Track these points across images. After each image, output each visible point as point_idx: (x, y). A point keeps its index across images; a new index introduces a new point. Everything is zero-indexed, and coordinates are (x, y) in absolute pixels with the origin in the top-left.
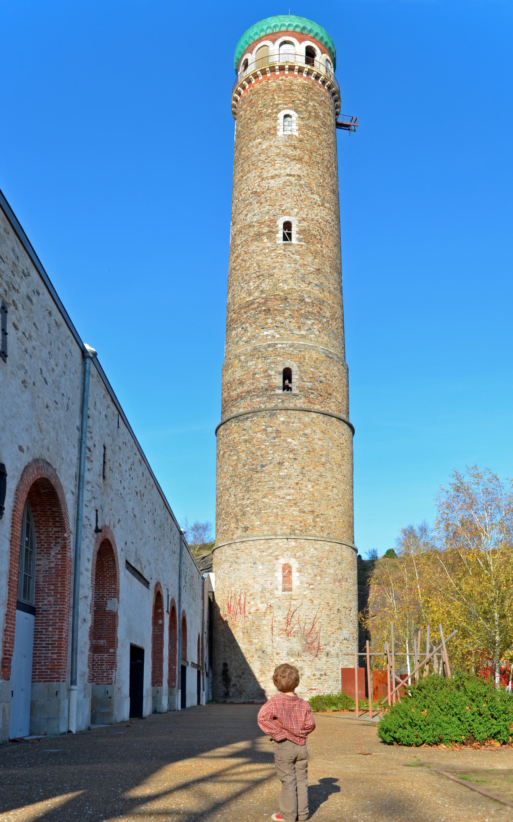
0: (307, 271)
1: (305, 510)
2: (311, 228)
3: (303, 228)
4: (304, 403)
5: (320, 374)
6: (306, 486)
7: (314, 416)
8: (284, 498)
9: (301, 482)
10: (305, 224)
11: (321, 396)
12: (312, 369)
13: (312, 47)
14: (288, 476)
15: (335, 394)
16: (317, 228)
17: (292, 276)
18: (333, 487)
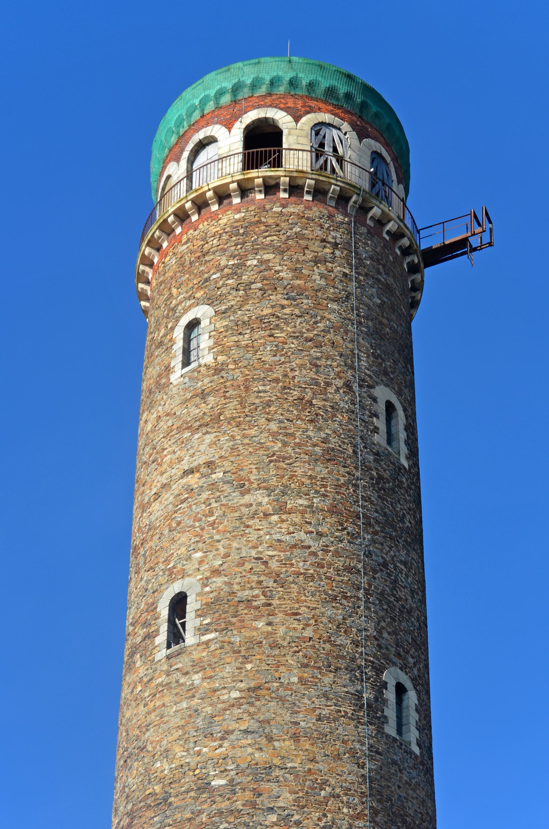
2: (236, 587)
3: (214, 594)
10: (219, 581)
13: (266, 119)
16: (255, 578)
17: (180, 732)
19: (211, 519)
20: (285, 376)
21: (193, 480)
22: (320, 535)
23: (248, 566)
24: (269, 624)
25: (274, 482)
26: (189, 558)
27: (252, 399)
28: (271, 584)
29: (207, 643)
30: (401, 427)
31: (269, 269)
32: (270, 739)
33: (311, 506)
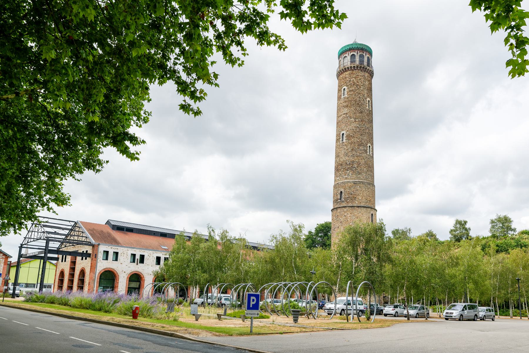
21: (345, 115)
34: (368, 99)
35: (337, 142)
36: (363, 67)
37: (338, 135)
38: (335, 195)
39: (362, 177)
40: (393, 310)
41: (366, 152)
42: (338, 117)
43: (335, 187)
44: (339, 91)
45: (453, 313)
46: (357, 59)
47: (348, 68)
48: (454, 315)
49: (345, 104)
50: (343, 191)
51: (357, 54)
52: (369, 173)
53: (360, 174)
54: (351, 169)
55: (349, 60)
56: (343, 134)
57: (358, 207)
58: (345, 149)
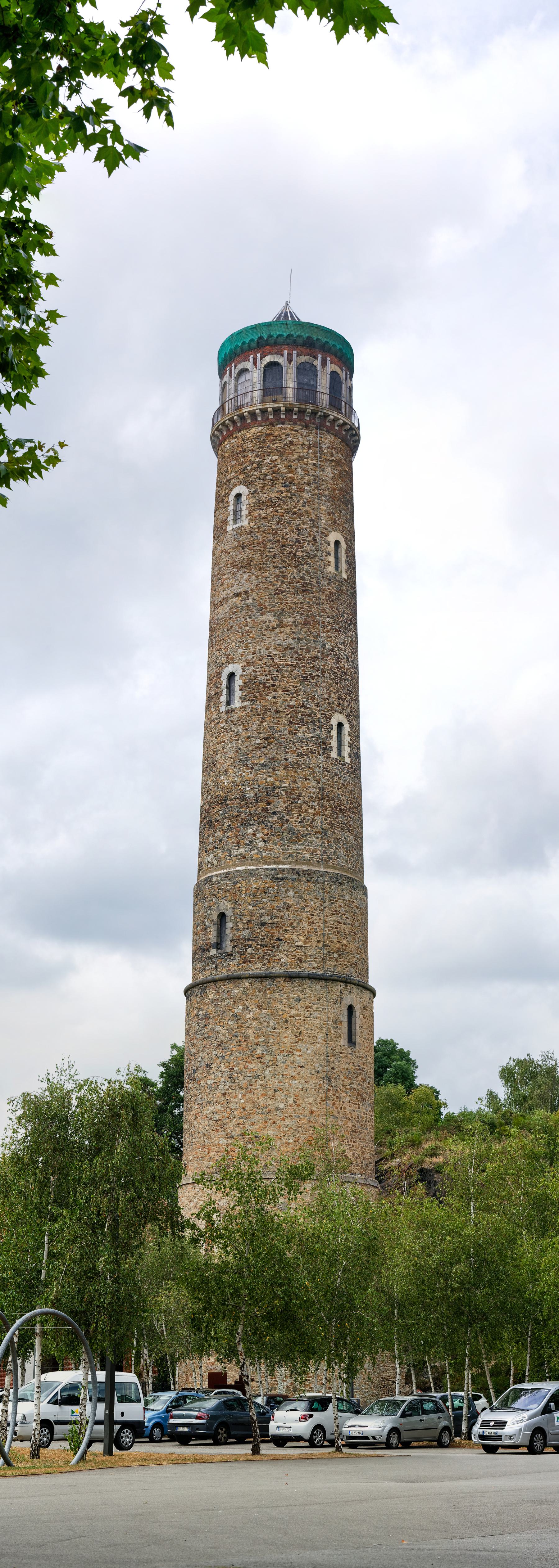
0: (251, 748)
1: (234, 1133)
4: (239, 965)
5: (262, 911)
6: (235, 1097)
7: (247, 984)
8: (211, 1119)
9: (230, 1091)
11: (263, 946)
12: (250, 908)
14: (215, 1086)
15: (288, 936)
16: (267, 669)
18: (275, 1091)
19: (247, 628)
20: (283, 538)
21: (238, 600)
22: (299, 639)
23: (264, 661)
24: (274, 697)
25: (277, 607)
26: (236, 652)
27: (266, 553)
28: (275, 672)
29: (245, 707)
30: (343, 552)
31: (275, 466)
32: (274, 770)
33: (294, 622)
34: (333, 536)
35: (208, 707)
36: (314, 413)
37: (213, 680)
38: (199, 927)
39: (308, 853)
40: (303, 1419)
41: (325, 747)
42: (214, 606)
43: (201, 892)
44: (221, 501)
45: (502, 1424)
46: (290, 381)
47: (253, 414)
48: (508, 1430)
49: (239, 556)
50: (229, 913)
51: (290, 359)
52: (338, 834)
53: (298, 838)
54: (262, 817)
55: (259, 386)
56: (232, 676)
57: (290, 977)
58: (237, 736)
